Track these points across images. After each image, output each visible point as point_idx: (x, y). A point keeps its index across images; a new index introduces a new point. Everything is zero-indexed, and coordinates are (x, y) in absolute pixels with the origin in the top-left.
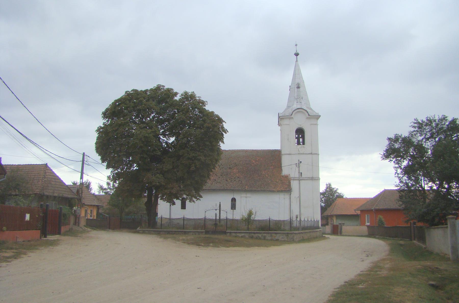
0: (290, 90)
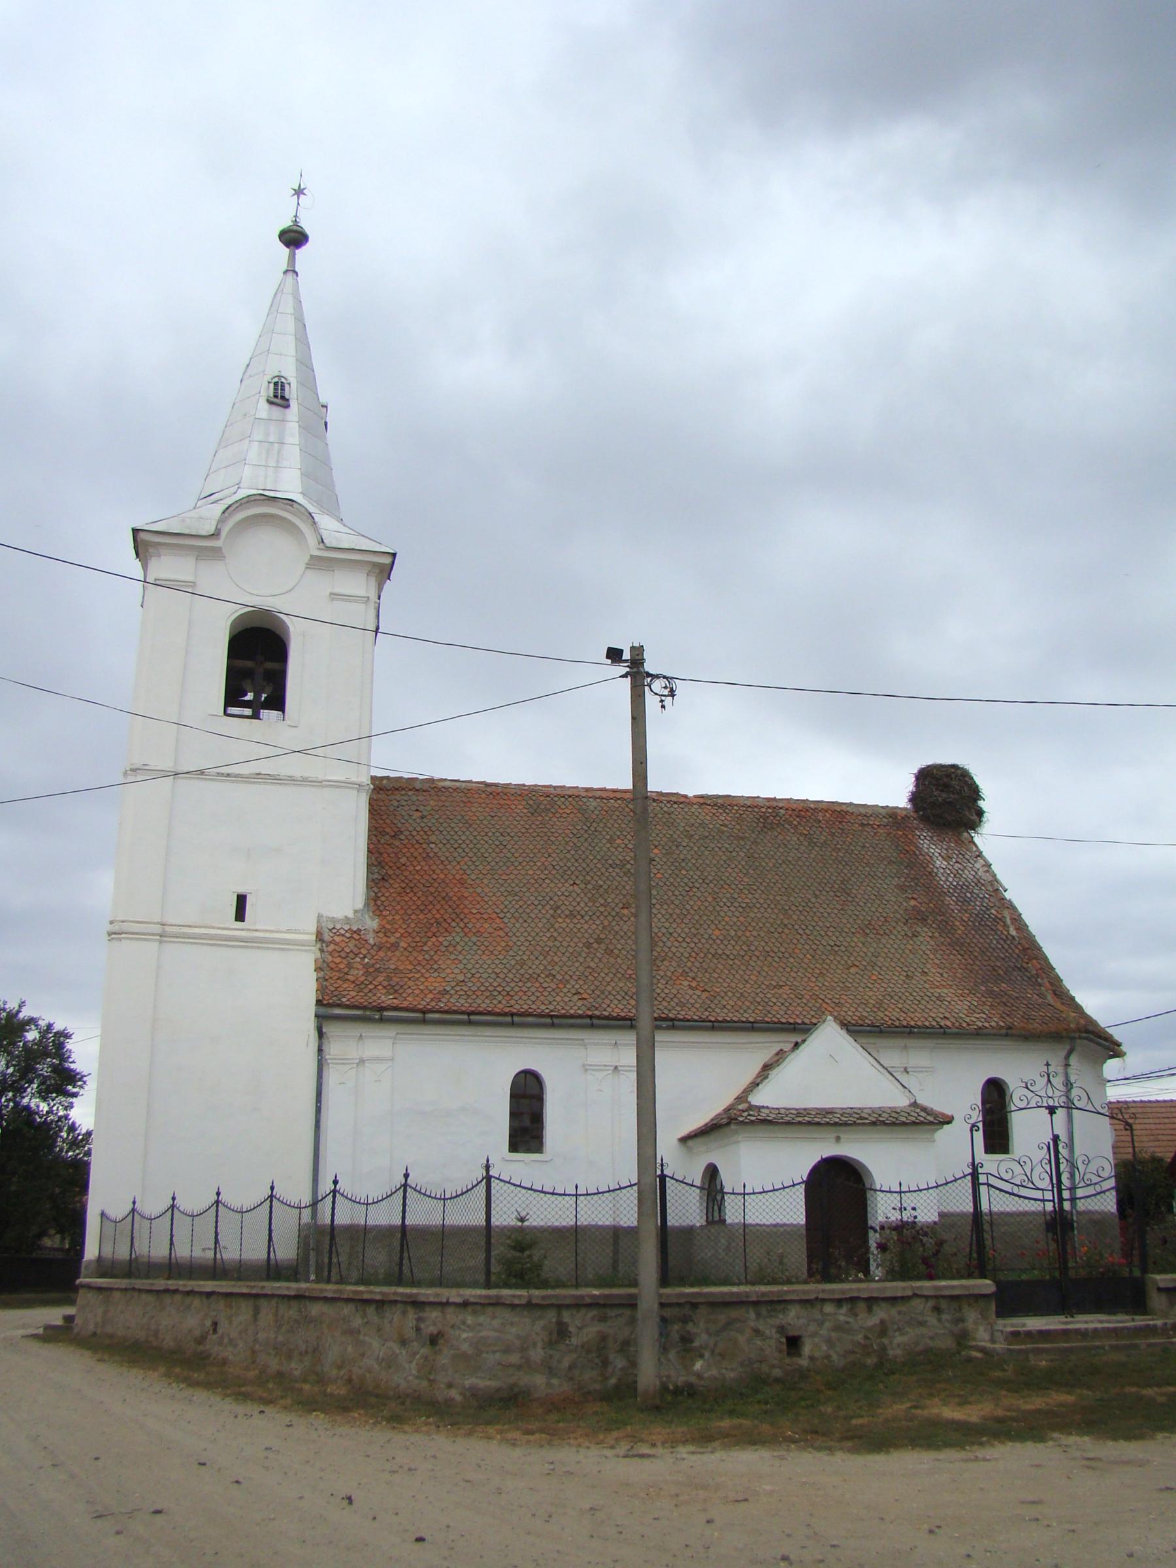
0: (326, 424)
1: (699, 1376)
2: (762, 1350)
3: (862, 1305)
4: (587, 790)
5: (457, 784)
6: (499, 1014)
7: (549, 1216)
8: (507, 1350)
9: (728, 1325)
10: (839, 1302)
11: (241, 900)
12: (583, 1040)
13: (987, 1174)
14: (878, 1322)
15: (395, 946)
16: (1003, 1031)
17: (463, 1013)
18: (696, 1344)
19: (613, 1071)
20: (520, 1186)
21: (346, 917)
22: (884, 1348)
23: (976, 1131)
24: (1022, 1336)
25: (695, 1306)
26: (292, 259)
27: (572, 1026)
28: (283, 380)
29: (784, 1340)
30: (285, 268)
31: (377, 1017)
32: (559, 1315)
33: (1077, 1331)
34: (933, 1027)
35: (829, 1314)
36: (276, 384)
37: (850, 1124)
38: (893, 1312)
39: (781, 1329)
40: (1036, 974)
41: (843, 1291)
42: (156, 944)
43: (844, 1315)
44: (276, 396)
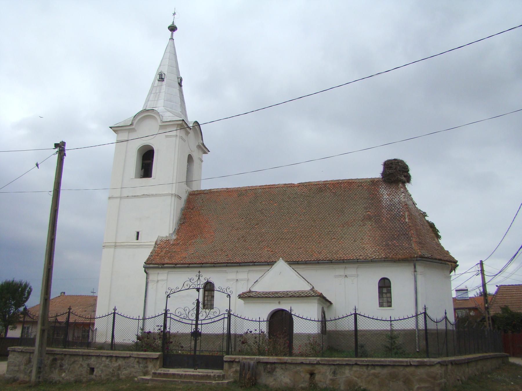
1: (63, 378)
2: (82, 371)
3: (114, 359)
4: (260, 186)
5: (218, 190)
6: (182, 264)
7: (213, 330)
8: (15, 366)
9: (74, 362)
10: (107, 357)
11: (138, 233)
12: (226, 271)
13: (171, 314)
14: (118, 365)
15: (178, 244)
16: (383, 259)
17: (187, 264)
18: (64, 368)
19: (236, 281)
20: (149, 318)
21: (166, 236)
22: (118, 375)
23: (169, 297)
24: (157, 374)
25: (65, 355)
26: (172, 35)
27: (220, 266)
28: (162, 73)
29: (89, 369)
30: (170, 38)
31: (160, 267)
32: (30, 355)
33: (178, 374)
34: (354, 259)
35: (103, 361)
36: (160, 75)
37: (281, 297)
38: (124, 362)
39: (88, 365)
40: (411, 236)
41: (108, 353)
42: (113, 249)
43: (109, 362)
44: (160, 78)
